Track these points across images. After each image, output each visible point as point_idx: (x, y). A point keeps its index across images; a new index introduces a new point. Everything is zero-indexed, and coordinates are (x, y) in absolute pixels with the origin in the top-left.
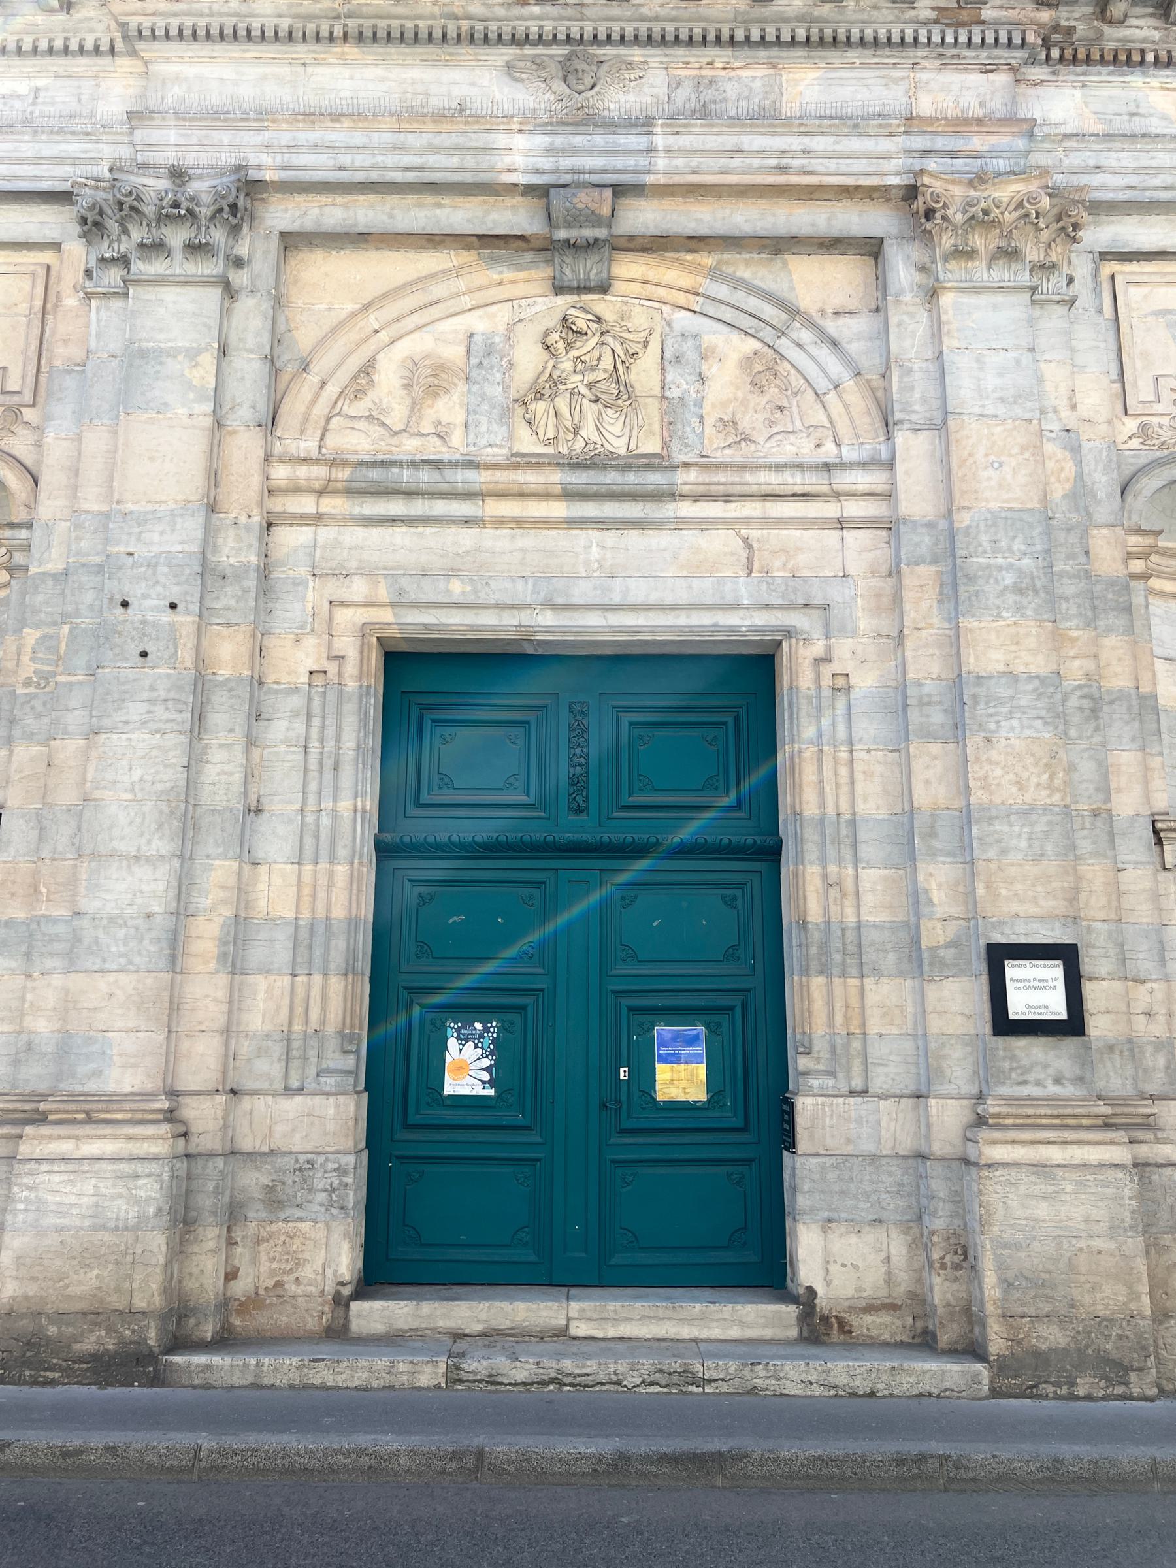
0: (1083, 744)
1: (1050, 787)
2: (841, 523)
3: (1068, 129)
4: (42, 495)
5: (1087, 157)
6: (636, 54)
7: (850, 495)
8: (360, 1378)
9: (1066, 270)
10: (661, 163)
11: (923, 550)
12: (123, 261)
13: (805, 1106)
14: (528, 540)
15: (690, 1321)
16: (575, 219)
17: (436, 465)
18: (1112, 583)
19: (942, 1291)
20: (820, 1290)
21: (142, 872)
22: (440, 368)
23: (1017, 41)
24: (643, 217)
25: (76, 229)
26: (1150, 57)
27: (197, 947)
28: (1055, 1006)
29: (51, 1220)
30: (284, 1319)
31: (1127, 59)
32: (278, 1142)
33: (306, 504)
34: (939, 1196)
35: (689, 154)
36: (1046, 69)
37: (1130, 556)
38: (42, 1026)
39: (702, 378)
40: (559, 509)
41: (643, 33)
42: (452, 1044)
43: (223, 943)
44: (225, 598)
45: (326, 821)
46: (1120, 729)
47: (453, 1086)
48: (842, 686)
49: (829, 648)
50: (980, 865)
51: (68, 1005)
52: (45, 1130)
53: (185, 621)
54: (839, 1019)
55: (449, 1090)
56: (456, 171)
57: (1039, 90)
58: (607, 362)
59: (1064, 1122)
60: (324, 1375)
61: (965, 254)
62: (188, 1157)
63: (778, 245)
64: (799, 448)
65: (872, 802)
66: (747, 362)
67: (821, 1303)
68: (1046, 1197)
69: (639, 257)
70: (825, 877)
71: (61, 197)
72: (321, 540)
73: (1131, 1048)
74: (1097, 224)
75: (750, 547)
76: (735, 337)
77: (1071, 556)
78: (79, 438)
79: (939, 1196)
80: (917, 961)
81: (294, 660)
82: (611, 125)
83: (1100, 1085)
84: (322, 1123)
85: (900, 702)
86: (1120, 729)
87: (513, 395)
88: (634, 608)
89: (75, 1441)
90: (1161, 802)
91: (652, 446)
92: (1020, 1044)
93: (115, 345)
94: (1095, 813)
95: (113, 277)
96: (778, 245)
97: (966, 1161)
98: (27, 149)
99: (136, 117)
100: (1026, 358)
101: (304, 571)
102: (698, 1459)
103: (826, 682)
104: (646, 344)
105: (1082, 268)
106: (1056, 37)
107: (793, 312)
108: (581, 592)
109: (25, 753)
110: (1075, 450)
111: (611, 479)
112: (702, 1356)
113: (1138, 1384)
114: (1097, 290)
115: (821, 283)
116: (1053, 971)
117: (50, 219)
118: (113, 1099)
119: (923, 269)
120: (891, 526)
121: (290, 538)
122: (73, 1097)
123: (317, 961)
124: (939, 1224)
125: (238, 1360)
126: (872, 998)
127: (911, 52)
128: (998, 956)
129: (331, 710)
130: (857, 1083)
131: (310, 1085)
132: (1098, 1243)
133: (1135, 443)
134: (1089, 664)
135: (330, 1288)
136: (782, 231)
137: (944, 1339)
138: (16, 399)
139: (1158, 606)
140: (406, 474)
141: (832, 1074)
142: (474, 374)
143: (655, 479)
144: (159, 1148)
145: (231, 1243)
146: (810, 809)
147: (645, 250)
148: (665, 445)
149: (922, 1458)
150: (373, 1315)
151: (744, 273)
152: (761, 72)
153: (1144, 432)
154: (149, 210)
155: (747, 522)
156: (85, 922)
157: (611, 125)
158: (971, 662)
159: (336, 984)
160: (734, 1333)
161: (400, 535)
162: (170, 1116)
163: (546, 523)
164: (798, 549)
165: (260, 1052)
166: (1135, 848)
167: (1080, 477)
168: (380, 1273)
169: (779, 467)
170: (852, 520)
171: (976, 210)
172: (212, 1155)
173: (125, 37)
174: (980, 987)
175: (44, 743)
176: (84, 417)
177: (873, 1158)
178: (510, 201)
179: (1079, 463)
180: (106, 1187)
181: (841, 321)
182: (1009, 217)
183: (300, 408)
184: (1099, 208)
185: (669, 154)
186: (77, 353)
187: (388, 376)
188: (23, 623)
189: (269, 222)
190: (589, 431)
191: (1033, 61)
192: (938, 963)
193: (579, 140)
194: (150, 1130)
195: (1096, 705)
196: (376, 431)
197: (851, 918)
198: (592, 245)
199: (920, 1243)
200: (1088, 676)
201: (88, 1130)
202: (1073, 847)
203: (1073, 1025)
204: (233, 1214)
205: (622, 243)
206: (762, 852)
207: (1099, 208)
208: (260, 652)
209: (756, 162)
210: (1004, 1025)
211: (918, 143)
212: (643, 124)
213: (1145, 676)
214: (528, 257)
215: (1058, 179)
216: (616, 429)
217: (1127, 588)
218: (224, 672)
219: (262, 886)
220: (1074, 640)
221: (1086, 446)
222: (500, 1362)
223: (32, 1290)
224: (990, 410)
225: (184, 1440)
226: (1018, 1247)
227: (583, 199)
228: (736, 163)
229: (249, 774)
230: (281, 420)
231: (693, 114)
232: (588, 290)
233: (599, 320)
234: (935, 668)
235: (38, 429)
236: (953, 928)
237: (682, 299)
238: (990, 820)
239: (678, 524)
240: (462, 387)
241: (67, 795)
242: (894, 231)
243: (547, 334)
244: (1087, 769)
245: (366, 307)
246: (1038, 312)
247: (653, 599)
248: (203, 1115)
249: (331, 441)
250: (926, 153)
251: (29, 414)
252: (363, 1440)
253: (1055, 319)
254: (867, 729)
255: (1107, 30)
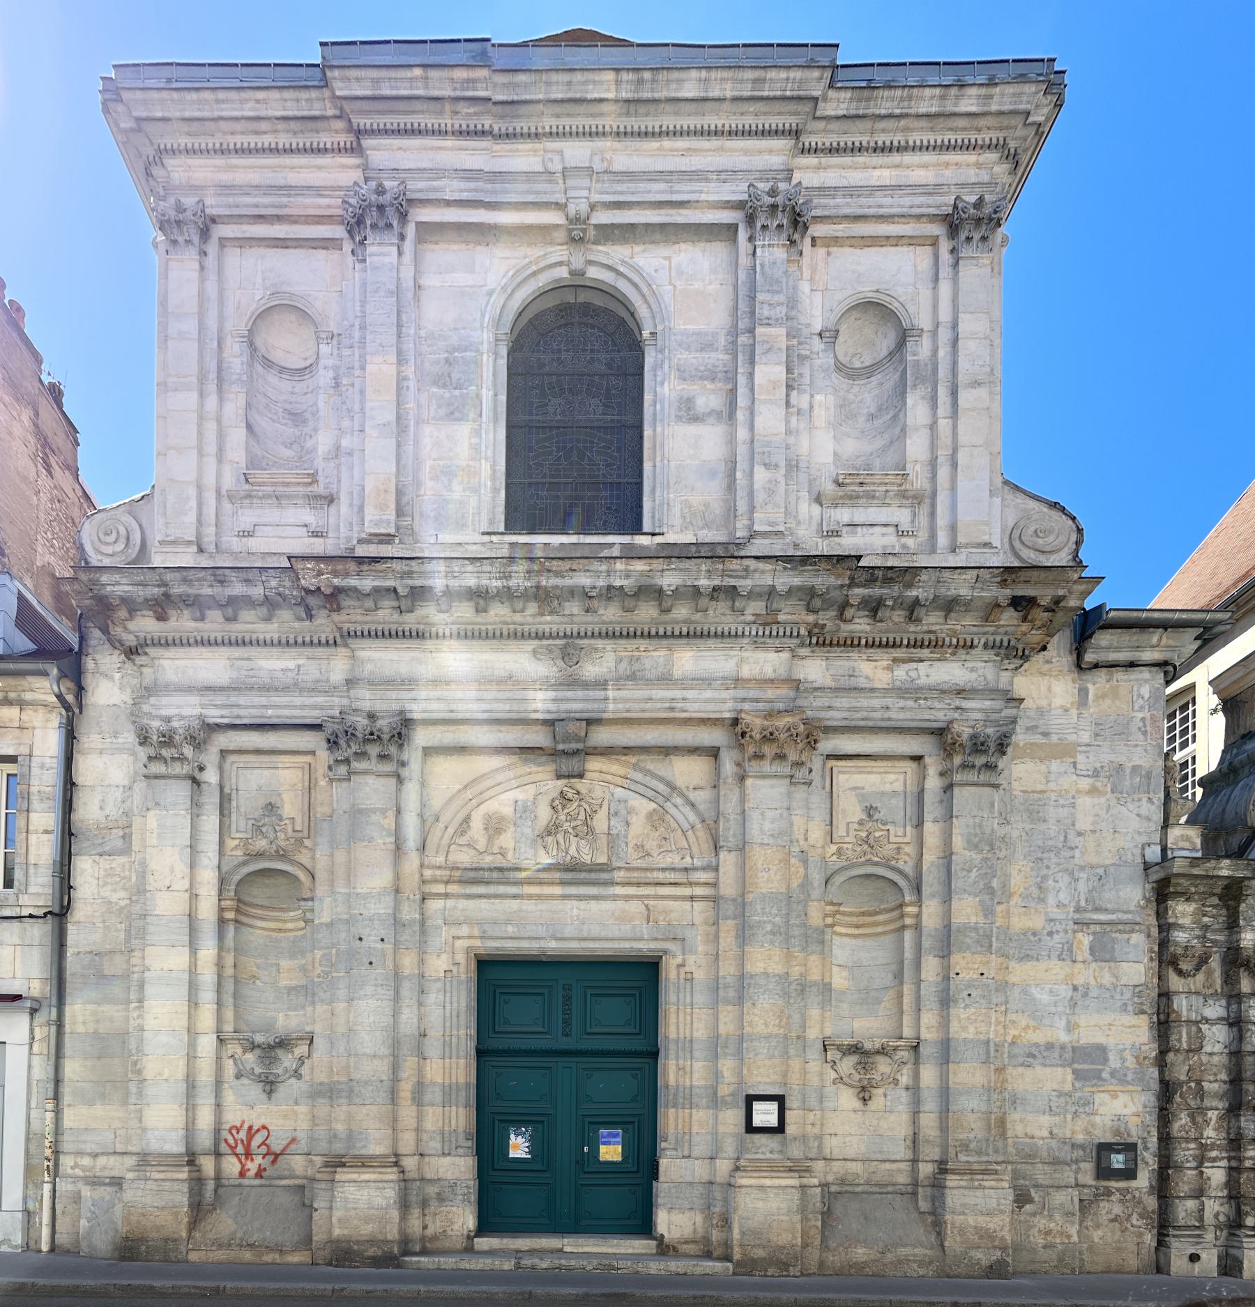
0: (796, 1006)
1: (779, 1026)
2: (692, 898)
3: (816, 685)
4: (317, 884)
5: (825, 701)
6: (600, 643)
7: (697, 884)
8: (480, 1266)
9: (809, 765)
10: (611, 707)
11: (730, 913)
12: (347, 761)
13: (663, 1162)
14: (543, 906)
15: (612, 1246)
16: (567, 738)
17: (501, 869)
18: (817, 929)
19: (716, 1235)
20: (666, 1235)
21: (377, 1062)
22: (501, 819)
23: (795, 634)
24: (602, 736)
25: (324, 745)
26: (863, 642)
27: (402, 1094)
28: (773, 1121)
29: (352, 1205)
30: (447, 1244)
31: (851, 644)
32: (441, 1175)
33: (440, 888)
34: (718, 1199)
35: (626, 701)
36: (808, 649)
37: (826, 915)
38: (340, 1127)
39: (628, 824)
40: (558, 890)
41: (604, 632)
42: (512, 1136)
43: (413, 1093)
44: (405, 936)
45: (454, 1040)
46: (813, 998)
47: (513, 1154)
48: (690, 979)
49: (684, 960)
50: (746, 1060)
51: (350, 1118)
52: (346, 1170)
53: (388, 947)
54: (680, 1126)
55: (511, 1155)
56: (509, 712)
57: (804, 662)
58: (582, 816)
59: (773, 1169)
60: (465, 1265)
61: (759, 757)
62: (405, 1181)
63: (667, 751)
64: (673, 859)
65: (701, 1032)
66: (650, 815)
67: (666, 1240)
68: (762, 1199)
69: (599, 758)
70: (677, 1065)
71: (316, 727)
72: (448, 906)
73: (804, 1139)
74: (827, 739)
75: (648, 909)
76: (644, 801)
77: (799, 916)
78: (332, 855)
79: (718, 1199)
80: (715, 1102)
81: (438, 964)
82: (586, 685)
83: (789, 1154)
84: (458, 1168)
85: (715, 987)
86: (813, 998)
87: (537, 833)
88: (594, 939)
89: (371, 1288)
90: (828, 1032)
91: (602, 859)
92: (757, 1137)
93: (346, 807)
94: (798, 1038)
95: (342, 770)
96: (667, 751)
97: (730, 1185)
98: (298, 701)
99: (350, 683)
100: (785, 814)
101: (440, 922)
102: (616, 1295)
103: (682, 976)
104: (601, 806)
105: (817, 763)
106: (816, 630)
107: (673, 788)
108: (568, 931)
109: (321, 1009)
110: (805, 862)
111: (583, 875)
112: (617, 1260)
113: (792, 1271)
114: (823, 777)
115: (688, 771)
116: (774, 1106)
117: (312, 739)
118: (373, 1157)
119: (738, 765)
120: (715, 900)
121: (434, 905)
122: (355, 1157)
123: (453, 1100)
124: (717, 1210)
125: (431, 1259)
126: (695, 1118)
127: (740, 640)
128: (750, 1100)
129: (455, 989)
130: (686, 1153)
131: (453, 1152)
132: (783, 1218)
133: (834, 858)
134: (802, 969)
135: (465, 1233)
136: (670, 744)
137: (715, 1254)
138: (300, 835)
139: (836, 940)
140: (487, 874)
141: (676, 1149)
142: (519, 822)
143: (605, 876)
144: (393, 1177)
145: (424, 1215)
146: (672, 1034)
147: (601, 754)
148: (609, 859)
149: (704, 1296)
150: (483, 1243)
151: (650, 766)
152: (663, 653)
153: (839, 852)
154: (360, 735)
155: (647, 897)
156: (354, 1084)
157: (586, 685)
158: (748, 968)
159: (462, 1111)
160: (630, 1251)
161: (483, 903)
162: (396, 1164)
163: (552, 897)
164: (672, 911)
165: (432, 1139)
166: (814, 1053)
167: (806, 876)
168: (484, 1228)
169: (664, 870)
170: (697, 896)
171: (767, 733)
172: (414, 1180)
173: (342, 636)
174: (742, 1112)
175: (329, 1004)
176: (333, 844)
177: (691, 1183)
178: (535, 728)
179: (806, 869)
180: (373, 1193)
181: (697, 793)
182: (783, 736)
183: (436, 840)
184: (828, 730)
185: (616, 701)
186: (327, 810)
187: (477, 823)
188: (314, 948)
189: (417, 741)
190: (572, 851)
191: (802, 645)
192: (725, 1103)
193: (570, 694)
194: (389, 1170)
195: (803, 988)
196: (473, 852)
197: (688, 1083)
198: (576, 753)
199: (708, 1218)
200: (801, 975)
201: (363, 1170)
202: (787, 1053)
203: (780, 1129)
204: (424, 1204)
205: (590, 751)
206: (649, 1054)
207: (828, 730)
208: (422, 961)
209: (659, 705)
210: (750, 1129)
211: (741, 693)
212: (602, 684)
213: (827, 974)
214: (544, 758)
215: (809, 714)
216: (586, 851)
217: (823, 931)
218: (407, 972)
219: (428, 1068)
220: (796, 957)
221: (811, 859)
222: (536, 1261)
223: (346, 1232)
224: (766, 841)
225: (415, 1287)
226: (749, 1219)
227: (572, 728)
228: (649, 706)
229: (420, 1019)
230: (427, 848)
231: (628, 678)
232: (573, 777)
233: (578, 793)
234: (732, 970)
235: (312, 850)
236: (731, 1088)
237: (619, 781)
238: (752, 1040)
239: (615, 898)
240: (512, 829)
241: (341, 1029)
242: (725, 743)
243: (553, 800)
244: (796, 1017)
245: (465, 787)
246: (793, 788)
247: (603, 934)
248: (409, 1163)
249: (450, 858)
250: (744, 700)
251: (307, 842)
252: (484, 1288)
253: (800, 792)
254: (700, 998)
255: (844, 627)
